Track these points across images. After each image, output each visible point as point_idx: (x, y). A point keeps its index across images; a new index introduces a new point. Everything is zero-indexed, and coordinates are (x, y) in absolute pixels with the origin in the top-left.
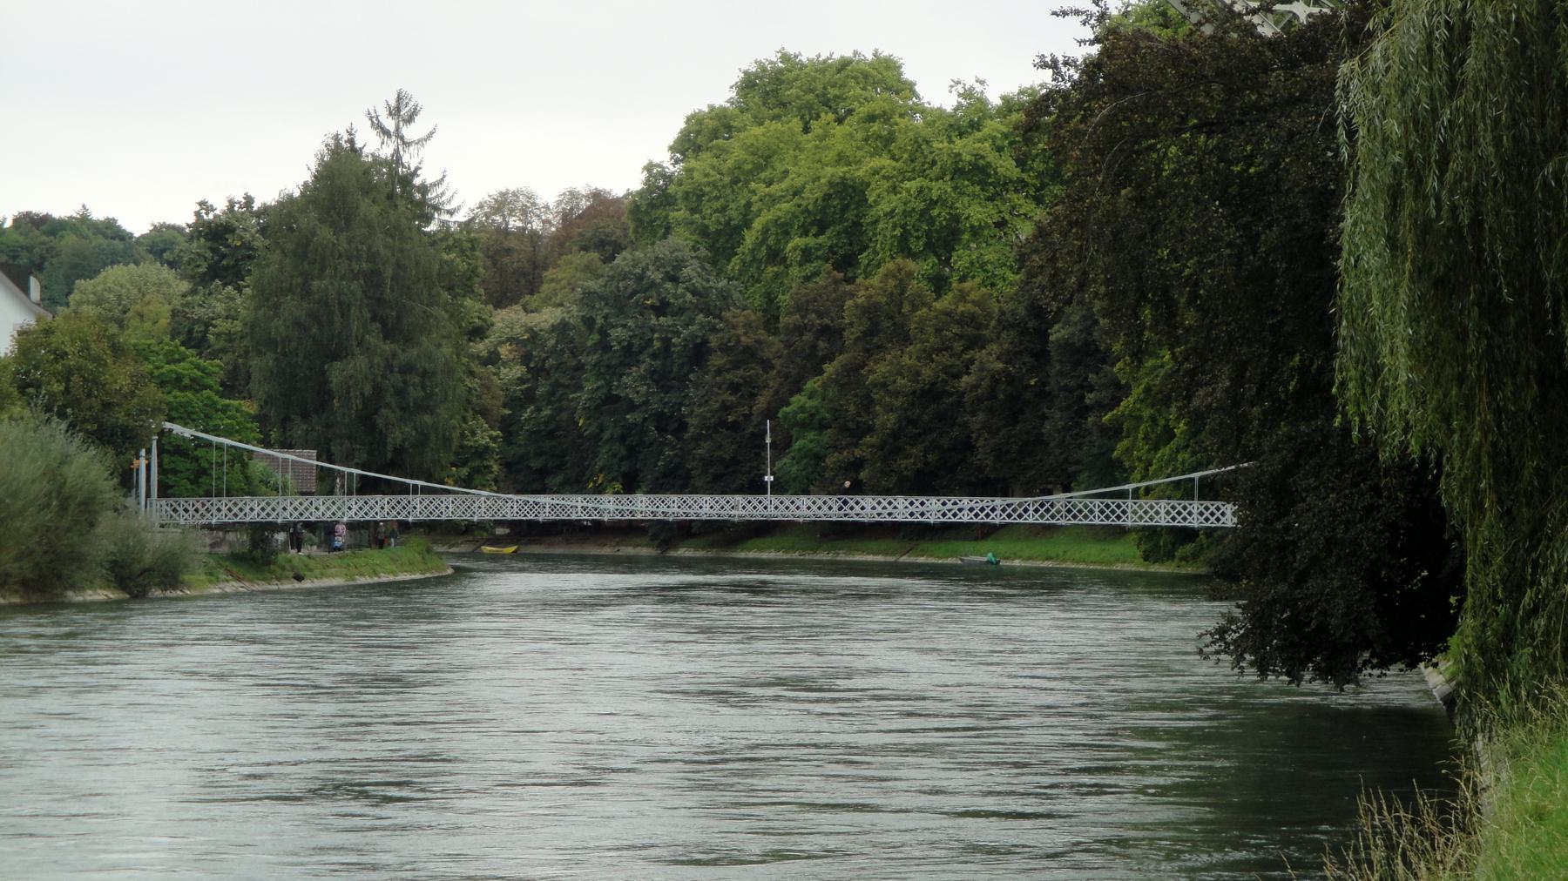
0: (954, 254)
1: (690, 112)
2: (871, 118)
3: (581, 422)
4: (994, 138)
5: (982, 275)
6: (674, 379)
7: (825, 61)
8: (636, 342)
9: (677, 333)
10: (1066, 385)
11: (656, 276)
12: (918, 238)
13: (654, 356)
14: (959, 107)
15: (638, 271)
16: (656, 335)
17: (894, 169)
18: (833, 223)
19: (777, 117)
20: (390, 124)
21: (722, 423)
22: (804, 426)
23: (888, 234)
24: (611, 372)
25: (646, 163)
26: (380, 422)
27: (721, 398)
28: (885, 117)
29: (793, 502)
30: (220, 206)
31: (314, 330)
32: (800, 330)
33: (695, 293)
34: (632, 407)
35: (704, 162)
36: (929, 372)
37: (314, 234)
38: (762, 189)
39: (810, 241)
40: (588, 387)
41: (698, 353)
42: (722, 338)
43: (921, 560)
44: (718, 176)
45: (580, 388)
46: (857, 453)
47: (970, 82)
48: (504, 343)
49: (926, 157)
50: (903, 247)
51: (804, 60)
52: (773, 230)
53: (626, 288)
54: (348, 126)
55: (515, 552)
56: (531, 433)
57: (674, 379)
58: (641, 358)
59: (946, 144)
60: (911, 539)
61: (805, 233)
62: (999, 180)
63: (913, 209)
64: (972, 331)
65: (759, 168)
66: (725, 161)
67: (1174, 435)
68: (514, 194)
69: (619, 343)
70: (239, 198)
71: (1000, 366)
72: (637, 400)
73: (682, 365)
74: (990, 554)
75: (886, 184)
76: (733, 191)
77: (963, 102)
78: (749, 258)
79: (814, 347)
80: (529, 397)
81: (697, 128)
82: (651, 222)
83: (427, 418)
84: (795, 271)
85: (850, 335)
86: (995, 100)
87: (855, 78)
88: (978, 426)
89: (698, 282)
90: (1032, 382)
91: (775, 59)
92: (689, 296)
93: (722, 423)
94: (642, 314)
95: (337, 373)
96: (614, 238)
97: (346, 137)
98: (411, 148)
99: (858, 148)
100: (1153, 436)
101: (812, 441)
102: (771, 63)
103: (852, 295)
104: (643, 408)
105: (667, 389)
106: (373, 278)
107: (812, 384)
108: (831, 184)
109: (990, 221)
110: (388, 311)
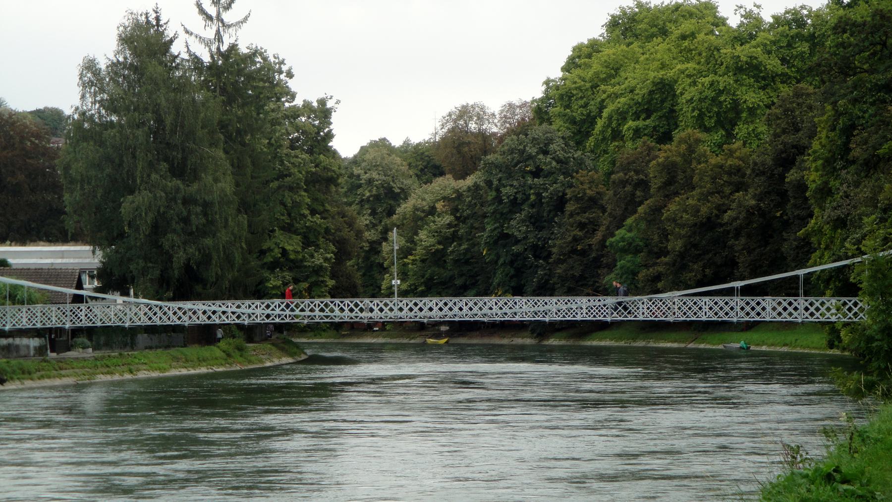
0: (737, 127)
1: (575, 44)
2: (684, 37)
3: (485, 252)
4: (765, 45)
5: (757, 142)
6: (545, 221)
8: (519, 196)
9: (546, 190)
10: (798, 215)
11: (532, 150)
12: (710, 117)
13: (532, 206)
14: (741, 25)
15: (521, 147)
18: (656, 111)
20: (212, 11)
21: (574, 251)
22: (625, 251)
23: (689, 115)
24: (504, 217)
25: (545, 79)
27: (572, 234)
29: (726, 303)
32: (623, 183)
33: (559, 161)
34: (517, 242)
36: (706, 209)
38: (610, 89)
39: (640, 123)
40: (489, 228)
41: (560, 203)
42: (574, 192)
43: (702, 346)
44: (583, 83)
45: (484, 230)
47: (750, 6)
48: (439, 200)
49: (716, 61)
51: (652, 6)
52: (615, 117)
54: (154, 7)
55: (447, 342)
56: (456, 261)
57: (545, 221)
60: (699, 331)
61: (637, 117)
62: (768, 74)
63: (707, 97)
68: (472, 106)
69: (508, 198)
71: (753, 202)
73: (550, 211)
74: (742, 342)
75: (689, 81)
76: (593, 94)
77: (745, 21)
78: (600, 137)
79: (633, 195)
80: (454, 237)
84: (629, 144)
86: (768, 18)
87: (683, 16)
88: (740, 248)
89: (561, 154)
91: (632, 6)
92: (554, 164)
93: (574, 251)
95: (128, 204)
97: (154, 15)
98: (230, 30)
99: (674, 58)
101: (628, 261)
104: (524, 242)
105: (540, 229)
109: (761, 104)
110: (175, 153)
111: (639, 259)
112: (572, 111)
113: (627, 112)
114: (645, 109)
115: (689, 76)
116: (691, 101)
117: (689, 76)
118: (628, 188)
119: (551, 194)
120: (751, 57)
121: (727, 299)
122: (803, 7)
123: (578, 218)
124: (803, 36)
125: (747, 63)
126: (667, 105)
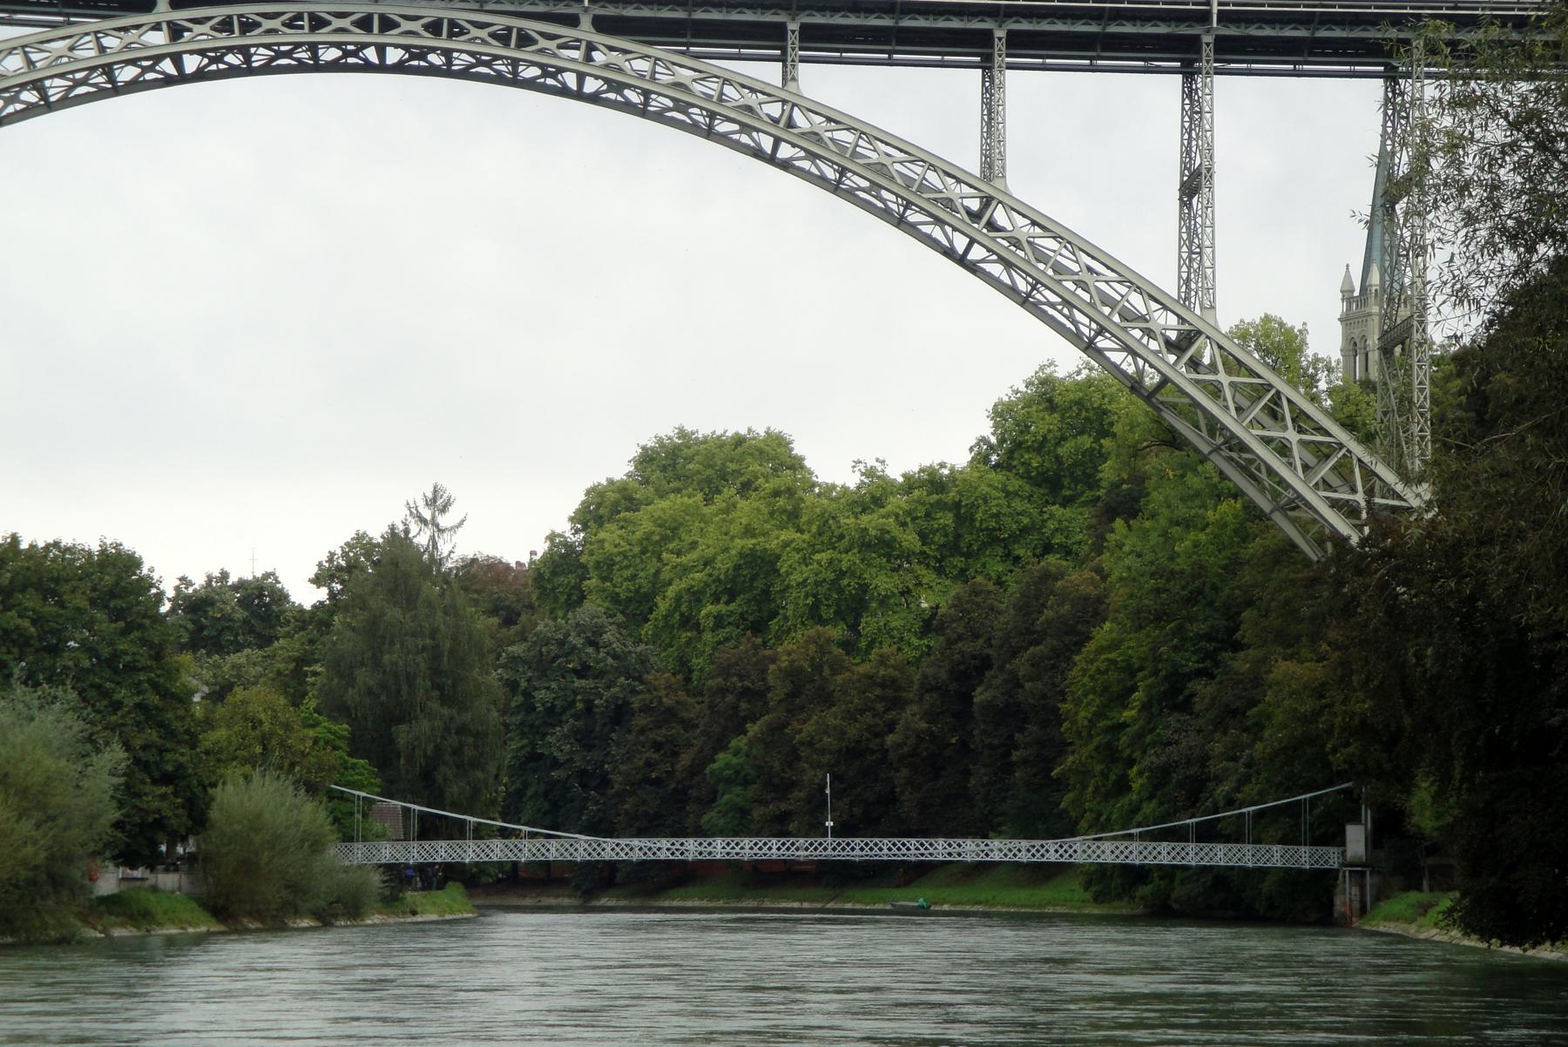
1: (589, 485)
2: (776, 493)
4: (897, 516)
7: (719, 437)
8: (558, 703)
9: (600, 696)
11: (576, 641)
12: (829, 606)
16: (579, 697)
17: (804, 541)
19: (678, 491)
20: (427, 514)
22: (729, 781)
23: (801, 602)
26: (439, 778)
28: (790, 492)
30: (199, 581)
31: (383, 698)
32: (723, 691)
33: (615, 656)
35: (610, 535)
37: (383, 614)
39: (721, 608)
41: (620, 713)
42: (644, 700)
46: (783, 807)
47: (871, 463)
50: (814, 614)
53: (548, 652)
58: (564, 718)
59: (853, 520)
61: (716, 600)
63: (825, 580)
64: (891, 692)
65: (665, 539)
66: (633, 532)
67: (1130, 789)
69: (543, 704)
70: (217, 574)
71: (924, 725)
72: (562, 757)
73: (605, 725)
74: (921, 900)
76: (642, 561)
79: (735, 708)
81: (599, 500)
82: (553, 589)
83: (479, 774)
84: (708, 636)
85: (773, 697)
90: (953, 741)
92: (610, 660)
94: (564, 677)
95: (403, 735)
96: (507, 603)
100: (1103, 790)
102: (670, 438)
103: (773, 660)
105: (589, 747)
106: (436, 652)
107: (738, 742)
108: (741, 555)
111: (751, 791)
112: (615, 586)
113: (701, 592)
114: (729, 589)
115: (798, 550)
116: (804, 583)
117: (798, 550)
118: (730, 698)
119: (607, 701)
120: (882, 530)
121: (1126, 843)
122: (942, 465)
123: (651, 736)
124: (946, 504)
125: (876, 537)
126: (759, 584)
